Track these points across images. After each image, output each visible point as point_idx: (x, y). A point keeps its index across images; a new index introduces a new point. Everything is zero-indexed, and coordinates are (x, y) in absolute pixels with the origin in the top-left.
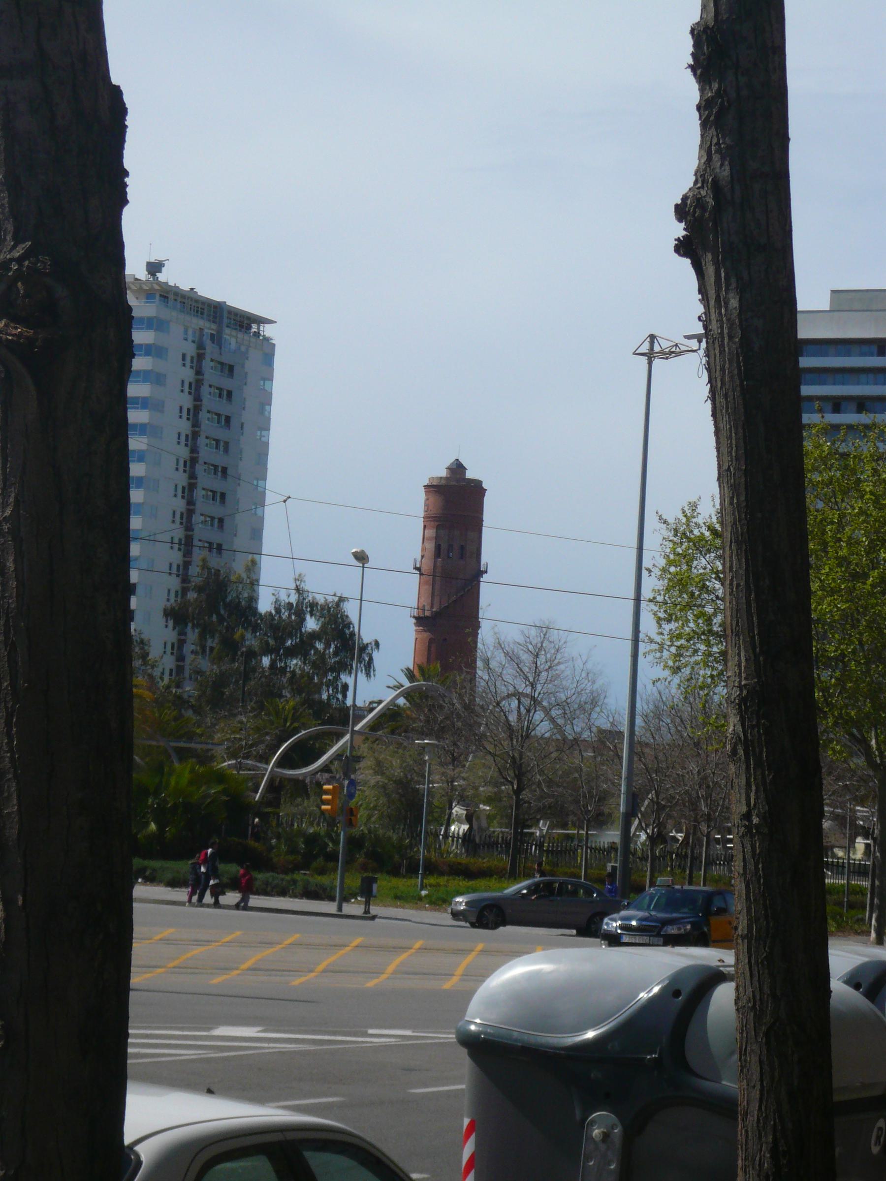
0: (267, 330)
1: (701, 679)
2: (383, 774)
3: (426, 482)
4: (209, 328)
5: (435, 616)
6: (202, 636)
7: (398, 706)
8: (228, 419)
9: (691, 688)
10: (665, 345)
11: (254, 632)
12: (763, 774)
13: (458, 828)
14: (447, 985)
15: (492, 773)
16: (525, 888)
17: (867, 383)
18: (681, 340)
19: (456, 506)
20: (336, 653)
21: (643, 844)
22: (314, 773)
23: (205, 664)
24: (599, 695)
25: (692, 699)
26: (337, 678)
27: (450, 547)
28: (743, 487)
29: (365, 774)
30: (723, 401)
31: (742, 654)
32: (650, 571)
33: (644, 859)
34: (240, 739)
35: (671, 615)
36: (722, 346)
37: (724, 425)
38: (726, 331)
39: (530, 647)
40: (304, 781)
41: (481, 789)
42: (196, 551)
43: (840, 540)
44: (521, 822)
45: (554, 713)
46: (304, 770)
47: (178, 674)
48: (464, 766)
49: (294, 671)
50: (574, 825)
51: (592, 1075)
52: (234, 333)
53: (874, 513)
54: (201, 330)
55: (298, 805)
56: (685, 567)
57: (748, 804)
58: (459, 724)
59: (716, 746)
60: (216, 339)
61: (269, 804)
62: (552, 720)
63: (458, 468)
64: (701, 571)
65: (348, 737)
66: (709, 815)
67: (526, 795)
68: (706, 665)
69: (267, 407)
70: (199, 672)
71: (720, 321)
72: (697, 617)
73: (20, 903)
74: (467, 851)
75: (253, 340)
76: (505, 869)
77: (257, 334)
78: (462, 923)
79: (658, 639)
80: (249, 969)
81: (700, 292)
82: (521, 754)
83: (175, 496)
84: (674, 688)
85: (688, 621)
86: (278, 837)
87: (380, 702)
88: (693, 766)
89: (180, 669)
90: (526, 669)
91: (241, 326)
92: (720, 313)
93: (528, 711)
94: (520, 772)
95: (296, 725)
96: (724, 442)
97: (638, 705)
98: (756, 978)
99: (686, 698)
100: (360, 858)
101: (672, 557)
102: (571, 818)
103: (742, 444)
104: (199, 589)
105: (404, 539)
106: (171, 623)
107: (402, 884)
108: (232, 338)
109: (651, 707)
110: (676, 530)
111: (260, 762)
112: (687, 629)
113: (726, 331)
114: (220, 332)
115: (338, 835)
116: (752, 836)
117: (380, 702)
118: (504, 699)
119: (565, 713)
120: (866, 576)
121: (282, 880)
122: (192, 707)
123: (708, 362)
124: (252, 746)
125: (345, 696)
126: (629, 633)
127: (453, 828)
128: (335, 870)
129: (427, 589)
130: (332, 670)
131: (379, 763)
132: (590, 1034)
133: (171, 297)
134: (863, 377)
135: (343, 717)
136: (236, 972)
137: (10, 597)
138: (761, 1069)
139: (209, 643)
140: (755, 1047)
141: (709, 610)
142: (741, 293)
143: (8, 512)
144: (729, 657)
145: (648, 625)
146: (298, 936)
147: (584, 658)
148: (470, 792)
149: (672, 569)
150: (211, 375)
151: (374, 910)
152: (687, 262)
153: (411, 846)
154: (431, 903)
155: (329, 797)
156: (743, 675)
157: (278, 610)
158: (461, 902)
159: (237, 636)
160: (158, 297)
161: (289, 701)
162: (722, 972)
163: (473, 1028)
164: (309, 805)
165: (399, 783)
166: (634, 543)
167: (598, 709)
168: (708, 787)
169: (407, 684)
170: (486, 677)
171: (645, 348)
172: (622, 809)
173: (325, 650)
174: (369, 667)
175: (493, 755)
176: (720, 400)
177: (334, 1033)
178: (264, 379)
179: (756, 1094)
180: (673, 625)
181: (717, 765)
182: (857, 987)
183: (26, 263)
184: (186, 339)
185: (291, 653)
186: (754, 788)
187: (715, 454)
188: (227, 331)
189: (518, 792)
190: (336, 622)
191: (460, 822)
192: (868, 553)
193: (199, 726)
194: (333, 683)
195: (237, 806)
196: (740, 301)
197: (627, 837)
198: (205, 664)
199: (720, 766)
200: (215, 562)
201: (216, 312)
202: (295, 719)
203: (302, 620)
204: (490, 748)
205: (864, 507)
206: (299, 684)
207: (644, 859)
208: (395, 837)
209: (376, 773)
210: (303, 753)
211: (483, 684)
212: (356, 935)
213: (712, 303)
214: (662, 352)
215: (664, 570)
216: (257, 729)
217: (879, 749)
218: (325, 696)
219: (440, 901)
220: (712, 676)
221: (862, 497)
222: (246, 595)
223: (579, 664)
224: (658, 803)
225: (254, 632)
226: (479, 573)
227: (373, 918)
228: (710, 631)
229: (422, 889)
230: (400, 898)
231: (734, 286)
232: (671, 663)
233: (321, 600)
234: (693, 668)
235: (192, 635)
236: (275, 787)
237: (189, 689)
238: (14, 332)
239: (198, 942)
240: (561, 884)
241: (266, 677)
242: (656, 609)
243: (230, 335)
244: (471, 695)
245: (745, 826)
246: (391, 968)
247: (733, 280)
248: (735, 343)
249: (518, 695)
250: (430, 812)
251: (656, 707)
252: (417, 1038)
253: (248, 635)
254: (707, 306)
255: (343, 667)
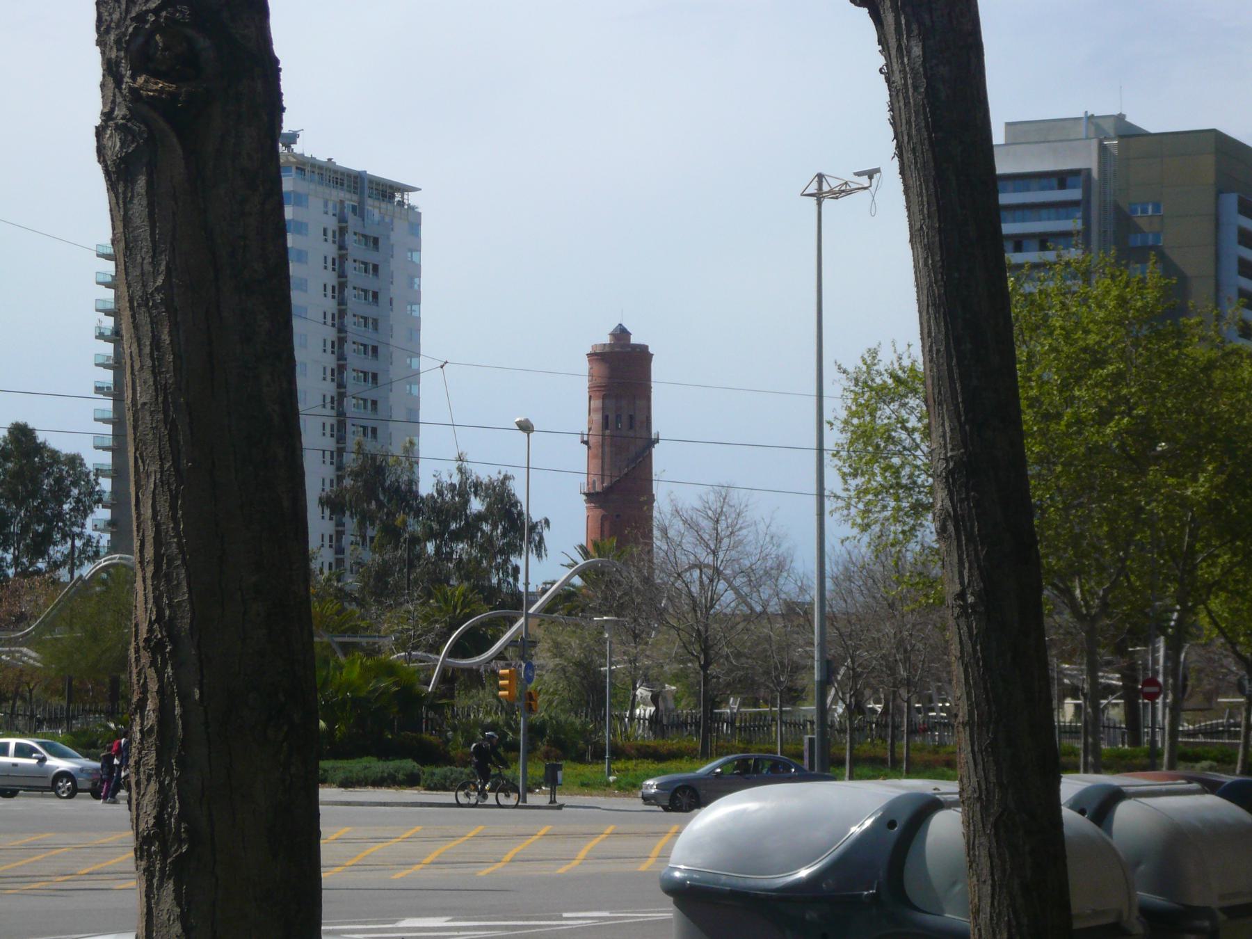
0: (412, 199)
1: (892, 536)
2: (561, 656)
3: (589, 350)
4: (350, 199)
5: (607, 492)
6: (362, 526)
7: (573, 586)
8: (375, 295)
9: (880, 547)
10: (834, 183)
11: (416, 516)
12: (976, 550)
13: (645, 711)
14: (643, 867)
15: (676, 648)
16: (720, 767)
17: (1049, 219)
18: (850, 177)
19: (622, 373)
20: (504, 535)
21: (840, 716)
22: (489, 661)
23: (368, 556)
24: (785, 560)
25: (883, 559)
26: (507, 561)
27: (618, 417)
28: (937, 244)
29: (543, 658)
30: (912, 157)
31: (947, 424)
32: (832, 424)
33: (842, 731)
34: (408, 630)
35: (856, 470)
36: (906, 98)
37: (914, 182)
38: (910, 81)
39: (710, 513)
40: (478, 671)
41: (666, 668)
42: (349, 436)
43: (1030, 379)
44: (711, 702)
45: (738, 582)
46: (477, 659)
47: (337, 566)
48: (646, 643)
49: (461, 559)
50: (766, 702)
51: (807, 917)
52: (377, 203)
53: (1065, 349)
54: (342, 202)
55: (472, 697)
56: (868, 418)
57: (962, 583)
58: (638, 600)
59: (912, 606)
60: (359, 210)
61: (443, 696)
62: (736, 591)
63: (621, 334)
64: (886, 421)
65: (522, 620)
66: (908, 679)
67: (713, 669)
68: (897, 520)
69: (416, 280)
70: (360, 564)
71: (903, 71)
72: (885, 470)
73: (197, 697)
74: (654, 733)
75: (397, 209)
76: (696, 749)
77: (401, 203)
78: (655, 808)
79: (844, 494)
80: (433, 863)
81: (880, 43)
82: (706, 627)
83: (324, 379)
84: (863, 547)
85: (874, 474)
86: (455, 729)
87: (553, 583)
88: (889, 629)
89: (340, 562)
90: (706, 537)
91: (384, 196)
92: (902, 62)
93: (711, 581)
94: (705, 646)
95: (467, 611)
96: (915, 199)
97: (827, 567)
98: (980, 767)
99: (877, 557)
100: (543, 747)
101: (854, 408)
102: (762, 692)
103: (934, 200)
104: (356, 475)
105: (571, 407)
106: (327, 512)
107: (588, 770)
108: (374, 208)
109: (841, 568)
110: (857, 380)
111: (431, 652)
112: (874, 484)
113: (910, 81)
114: (362, 203)
115: (518, 724)
116: (968, 616)
117: (553, 583)
118: (686, 570)
119: (750, 581)
120: (1059, 416)
121: (461, 773)
122: (355, 599)
123: (893, 117)
124: (420, 636)
125: (516, 579)
126: (813, 488)
127: (638, 711)
128: (516, 760)
129: (597, 463)
130: (502, 551)
131: (557, 645)
132: (803, 873)
133: (308, 169)
134: (1044, 213)
135: (517, 601)
136: (417, 867)
137: (167, 372)
138: (991, 863)
139: (371, 532)
140: (984, 840)
141: (896, 461)
142: (924, 41)
143: (160, 281)
144: (933, 429)
145: (833, 482)
146: (481, 828)
147: (767, 521)
148: (654, 672)
149: (855, 421)
150: (355, 248)
151: (560, 799)
152: (864, 11)
153: (595, 731)
154: (620, 788)
155: (506, 682)
156: (949, 446)
157: (440, 493)
158: (651, 785)
159: (398, 522)
160: (294, 170)
161: (457, 587)
162: (938, 800)
163: (677, 874)
164: (484, 696)
165: (579, 664)
166: (814, 391)
167: (785, 574)
168: (905, 651)
169: (581, 562)
170: (665, 547)
171: (813, 188)
172: (816, 677)
173: (492, 531)
174: (540, 547)
175: (678, 629)
176: (908, 155)
177: (527, 919)
178: (412, 251)
179: (987, 889)
180: (860, 480)
181: (914, 626)
182: (1082, 812)
183: (164, 14)
184: (326, 213)
185: (457, 536)
186: (967, 565)
187: (906, 214)
188: (370, 201)
189: (705, 667)
190: (502, 501)
191: (646, 704)
192: (1061, 392)
193: (364, 619)
194: (503, 567)
195: (408, 697)
196: (924, 48)
197: (823, 711)
198: (368, 556)
199: (919, 627)
200: (370, 446)
201: (355, 182)
202: (464, 606)
203: (466, 502)
204: (674, 622)
205: (1055, 344)
206: (469, 570)
207: (842, 731)
208: (578, 722)
209: (555, 656)
210: (475, 642)
211: (662, 554)
212: (546, 823)
213: (893, 52)
214: (831, 192)
215: (846, 422)
216: (426, 618)
217: (1084, 599)
218: (494, 581)
219: (630, 786)
220: (903, 532)
221: (1051, 334)
222: (406, 478)
223: (762, 527)
224: (853, 669)
225: (416, 516)
226: (651, 443)
227: (560, 807)
228: (898, 484)
229: (609, 775)
230: (586, 786)
231: (916, 32)
232: (859, 521)
233: (486, 480)
234: (883, 524)
235: (351, 524)
236: (448, 678)
237: (352, 582)
238: (155, 87)
239: (377, 840)
240: (757, 760)
241: (433, 563)
242: (840, 463)
243: (373, 206)
244: (650, 567)
245: (960, 606)
246: (582, 855)
247: (915, 27)
248: (920, 94)
249: (700, 566)
250: (613, 696)
251: (847, 569)
252: (616, 918)
253: (411, 520)
254: (888, 57)
255: (514, 548)
